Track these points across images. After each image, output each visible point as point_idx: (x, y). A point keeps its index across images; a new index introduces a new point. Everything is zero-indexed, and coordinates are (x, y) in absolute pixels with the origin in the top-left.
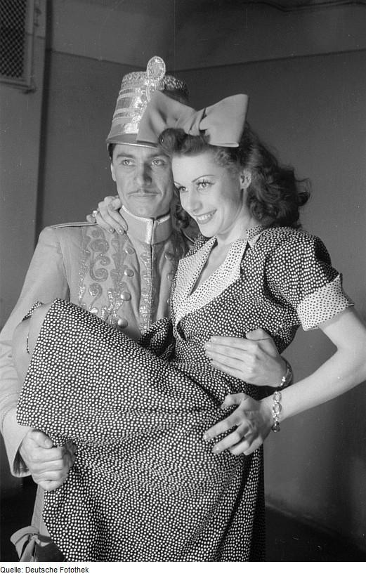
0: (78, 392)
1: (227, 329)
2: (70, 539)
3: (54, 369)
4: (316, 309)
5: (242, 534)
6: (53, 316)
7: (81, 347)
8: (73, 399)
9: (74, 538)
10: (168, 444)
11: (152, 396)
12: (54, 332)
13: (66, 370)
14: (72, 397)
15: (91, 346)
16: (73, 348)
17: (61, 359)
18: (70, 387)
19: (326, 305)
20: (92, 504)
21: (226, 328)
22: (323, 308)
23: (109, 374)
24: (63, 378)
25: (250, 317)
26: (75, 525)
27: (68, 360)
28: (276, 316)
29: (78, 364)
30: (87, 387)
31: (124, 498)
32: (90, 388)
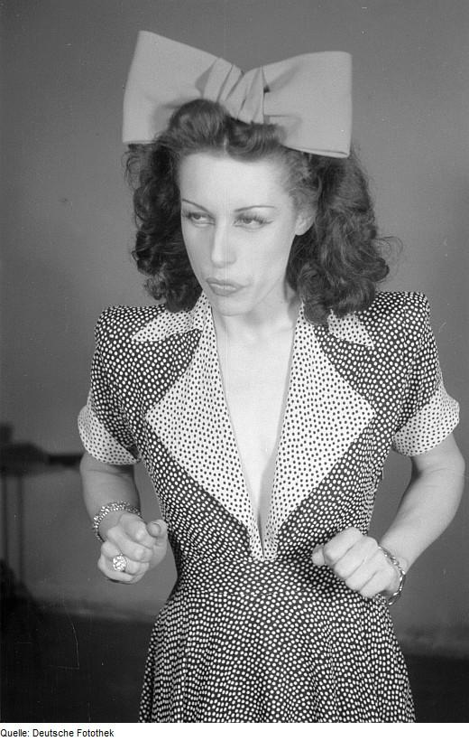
3: (392, 334)
4: (192, 439)
5: (236, 662)
6: (386, 355)
7: (149, 381)
8: (384, 324)
12: (243, 640)
15: (153, 365)
16: (246, 649)
17: (265, 635)
20: (252, 616)
22: (193, 428)
23: (398, 342)
24: (268, 603)
25: (215, 584)
26: (142, 369)
28: (399, 309)
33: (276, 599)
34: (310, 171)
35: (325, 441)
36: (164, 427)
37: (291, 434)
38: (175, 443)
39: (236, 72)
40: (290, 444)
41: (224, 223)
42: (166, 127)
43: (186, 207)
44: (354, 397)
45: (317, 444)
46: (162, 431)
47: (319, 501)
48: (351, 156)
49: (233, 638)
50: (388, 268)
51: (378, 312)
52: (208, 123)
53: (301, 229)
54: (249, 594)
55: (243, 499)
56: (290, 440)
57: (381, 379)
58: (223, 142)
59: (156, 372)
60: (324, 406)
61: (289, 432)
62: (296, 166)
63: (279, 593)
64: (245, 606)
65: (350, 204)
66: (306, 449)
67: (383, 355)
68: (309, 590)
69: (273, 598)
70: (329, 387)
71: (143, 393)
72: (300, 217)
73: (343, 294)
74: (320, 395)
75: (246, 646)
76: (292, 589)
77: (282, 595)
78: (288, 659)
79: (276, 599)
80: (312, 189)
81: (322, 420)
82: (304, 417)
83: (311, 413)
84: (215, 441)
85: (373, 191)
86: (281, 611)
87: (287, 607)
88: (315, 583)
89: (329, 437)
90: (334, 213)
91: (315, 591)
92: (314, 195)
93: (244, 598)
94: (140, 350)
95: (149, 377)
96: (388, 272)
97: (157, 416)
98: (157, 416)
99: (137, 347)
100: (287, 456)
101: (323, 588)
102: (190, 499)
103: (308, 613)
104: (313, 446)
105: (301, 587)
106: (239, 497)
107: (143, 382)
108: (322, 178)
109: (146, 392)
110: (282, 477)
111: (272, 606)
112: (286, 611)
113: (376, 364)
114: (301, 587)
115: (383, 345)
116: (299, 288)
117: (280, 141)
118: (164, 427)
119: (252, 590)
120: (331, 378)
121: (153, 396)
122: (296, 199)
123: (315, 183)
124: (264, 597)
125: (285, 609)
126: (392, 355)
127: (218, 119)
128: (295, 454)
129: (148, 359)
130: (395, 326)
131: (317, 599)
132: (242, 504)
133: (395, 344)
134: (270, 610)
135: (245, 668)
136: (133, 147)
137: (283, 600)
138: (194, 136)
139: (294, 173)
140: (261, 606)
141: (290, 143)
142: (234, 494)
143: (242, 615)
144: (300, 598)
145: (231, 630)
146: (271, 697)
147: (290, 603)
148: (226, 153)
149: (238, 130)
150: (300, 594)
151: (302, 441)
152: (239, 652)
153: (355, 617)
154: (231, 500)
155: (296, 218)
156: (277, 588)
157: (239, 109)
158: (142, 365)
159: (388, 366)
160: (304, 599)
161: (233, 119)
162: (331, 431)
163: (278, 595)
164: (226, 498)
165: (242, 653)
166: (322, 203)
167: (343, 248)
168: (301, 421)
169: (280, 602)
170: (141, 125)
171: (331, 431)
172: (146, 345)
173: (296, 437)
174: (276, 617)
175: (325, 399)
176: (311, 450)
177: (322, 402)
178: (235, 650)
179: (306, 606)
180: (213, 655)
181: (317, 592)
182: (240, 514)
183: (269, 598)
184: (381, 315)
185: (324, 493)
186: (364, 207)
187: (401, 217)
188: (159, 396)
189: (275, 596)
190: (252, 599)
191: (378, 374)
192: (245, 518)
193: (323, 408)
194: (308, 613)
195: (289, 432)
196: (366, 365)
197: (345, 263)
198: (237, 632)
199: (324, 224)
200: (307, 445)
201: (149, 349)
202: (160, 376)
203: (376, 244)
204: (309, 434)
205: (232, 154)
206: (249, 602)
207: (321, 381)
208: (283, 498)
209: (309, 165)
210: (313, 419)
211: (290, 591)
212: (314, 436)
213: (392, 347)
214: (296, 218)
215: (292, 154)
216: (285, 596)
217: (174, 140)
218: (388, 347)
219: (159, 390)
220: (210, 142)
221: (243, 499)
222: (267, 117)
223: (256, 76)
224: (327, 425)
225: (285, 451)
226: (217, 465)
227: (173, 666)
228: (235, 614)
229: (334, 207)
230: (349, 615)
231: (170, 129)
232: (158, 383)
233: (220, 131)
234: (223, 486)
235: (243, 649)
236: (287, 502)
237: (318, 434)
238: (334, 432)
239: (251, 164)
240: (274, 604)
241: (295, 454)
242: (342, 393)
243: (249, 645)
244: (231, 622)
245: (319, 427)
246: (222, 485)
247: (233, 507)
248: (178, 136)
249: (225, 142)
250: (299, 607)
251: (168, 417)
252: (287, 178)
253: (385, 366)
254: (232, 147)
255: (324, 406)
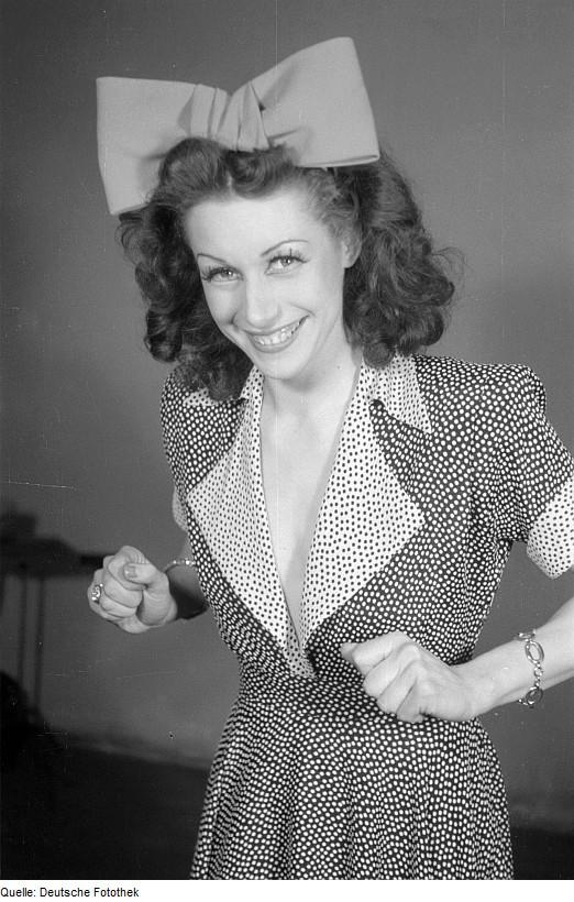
0: (456, 422)
1: (320, 770)
2: (482, 446)
3: (456, 422)
6: (444, 448)
7: (195, 451)
9: (204, 455)
10: (432, 501)
11: (400, 564)
13: (443, 443)
14: (452, 407)
15: (203, 433)
18: (356, 612)
19: (242, 561)
21: (323, 767)
26: (189, 437)
27: (460, 456)
29: (445, 470)
30: (454, 443)
31: (338, 736)
32: (449, 447)
33: (323, 723)
34: (338, 187)
35: (362, 550)
36: (203, 510)
37: (321, 537)
38: (211, 531)
39: (222, 95)
40: (351, 494)
41: (254, 276)
42: (156, 182)
43: (205, 264)
44: (401, 498)
45: (351, 551)
46: (201, 515)
47: (322, 761)
48: (382, 158)
49: (254, 824)
50: (451, 284)
51: (380, 617)
52: (200, 163)
53: (346, 262)
54: (296, 712)
55: (274, 603)
56: (350, 490)
57: (437, 537)
58: (226, 181)
59: (205, 442)
60: (367, 506)
61: (350, 479)
62: (321, 186)
63: (328, 717)
64: (268, 786)
65: (396, 217)
66: (338, 557)
67: (440, 448)
68: (364, 721)
69: (320, 722)
70: (316, 592)
71: (187, 464)
72: (343, 243)
73: (403, 326)
74: (334, 547)
75: (268, 833)
76: (343, 715)
77: (331, 720)
78: (385, 607)
79: (323, 723)
80: (348, 209)
81: (362, 523)
82: (340, 518)
83: (319, 568)
84: (247, 532)
85: (419, 197)
86: (326, 739)
87: (334, 735)
88: (373, 714)
89: (368, 545)
90: (376, 231)
91: (371, 723)
92: (350, 216)
93: (289, 716)
94: (191, 415)
95: (196, 447)
96: (453, 291)
97: (198, 497)
98: (198, 497)
99: (188, 411)
100: (345, 509)
101: (383, 722)
102: (222, 596)
103: (356, 747)
104: (346, 554)
105: (354, 715)
106: (269, 601)
107: (188, 452)
108: (355, 191)
109: (190, 464)
110: (337, 533)
111: (318, 731)
112: (332, 740)
113: (392, 837)
114: (354, 715)
115: (437, 556)
116: (354, 326)
117: (295, 164)
118: (203, 510)
119: (299, 708)
120: (351, 527)
121: (197, 470)
122: (331, 226)
123: (350, 200)
124: (310, 718)
125: (331, 737)
126: (453, 449)
127: (215, 157)
128: (324, 560)
129: (197, 426)
130: (452, 536)
131: (372, 734)
132: (272, 609)
133: (458, 435)
134: (313, 734)
135: (302, 739)
136: (127, 217)
137: (330, 726)
138: (191, 184)
139: (322, 194)
140: (305, 728)
141: (306, 161)
142: (264, 597)
143: (264, 797)
144: (351, 727)
145: (251, 813)
146: (373, 609)
147: (338, 732)
148: (232, 193)
149: (242, 162)
150: (351, 723)
151: (364, 492)
152: (260, 839)
153: (420, 766)
154: (260, 604)
155: (338, 247)
156: (326, 711)
157: (235, 138)
158: (190, 433)
159: (446, 463)
160: (355, 730)
161: (233, 152)
162: (372, 538)
163: (326, 720)
164: (253, 600)
165: (263, 841)
166: (363, 222)
167: (392, 272)
168: (335, 522)
169: (327, 728)
170: (126, 186)
171: (372, 538)
172: (198, 409)
173: (328, 540)
174: (319, 744)
175: (369, 498)
176: (344, 558)
177: (365, 501)
178: (255, 838)
179: (356, 738)
180: (250, 774)
181: (374, 725)
182: (269, 621)
183: (316, 721)
184: (384, 621)
185: (330, 768)
186: (411, 219)
187: (481, 229)
188: (205, 470)
189: (323, 719)
190: (298, 719)
191: (433, 531)
192: (275, 626)
193: (335, 563)
194: (356, 747)
195: (350, 479)
196: (432, 397)
197: (397, 288)
198: (258, 816)
199: (368, 248)
200: (339, 553)
201: (201, 414)
202: (208, 447)
203: (433, 260)
204: (343, 539)
205: (241, 192)
206: (295, 721)
207: (338, 529)
208: (336, 561)
209: (336, 181)
210: (351, 521)
211: (340, 717)
212: (350, 542)
213: (453, 438)
214: (338, 247)
215: (313, 173)
216: (334, 721)
217: (171, 195)
218: (448, 438)
219: (205, 464)
220: (211, 186)
221: (274, 603)
222: (270, 140)
223: (247, 92)
224: (367, 530)
225: (344, 503)
226: (249, 560)
227: (234, 723)
228: (256, 795)
229: (375, 225)
230: (414, 762)
231: (162, 184)
232: (204, 455)
233: (220, 170)
234: (253, 585)
235: (264, 837)
236: (341, 566)
237: (355, 540)
238: (374, 539)
239: (268, 198)
240: (320, 729)
241: (324, 560)
242: (362, 548)
243: (272, 832)
244: (252, 804)
245: (357, 531)
246: (251, 585)
247: (261, 612)
248: (173, 189)
249: (230, 180)
250: (348, 738)
251: (209, 499)
252: (313, 204)
253: (441, 523)
254: (239, 186)
255: (336, 561)
